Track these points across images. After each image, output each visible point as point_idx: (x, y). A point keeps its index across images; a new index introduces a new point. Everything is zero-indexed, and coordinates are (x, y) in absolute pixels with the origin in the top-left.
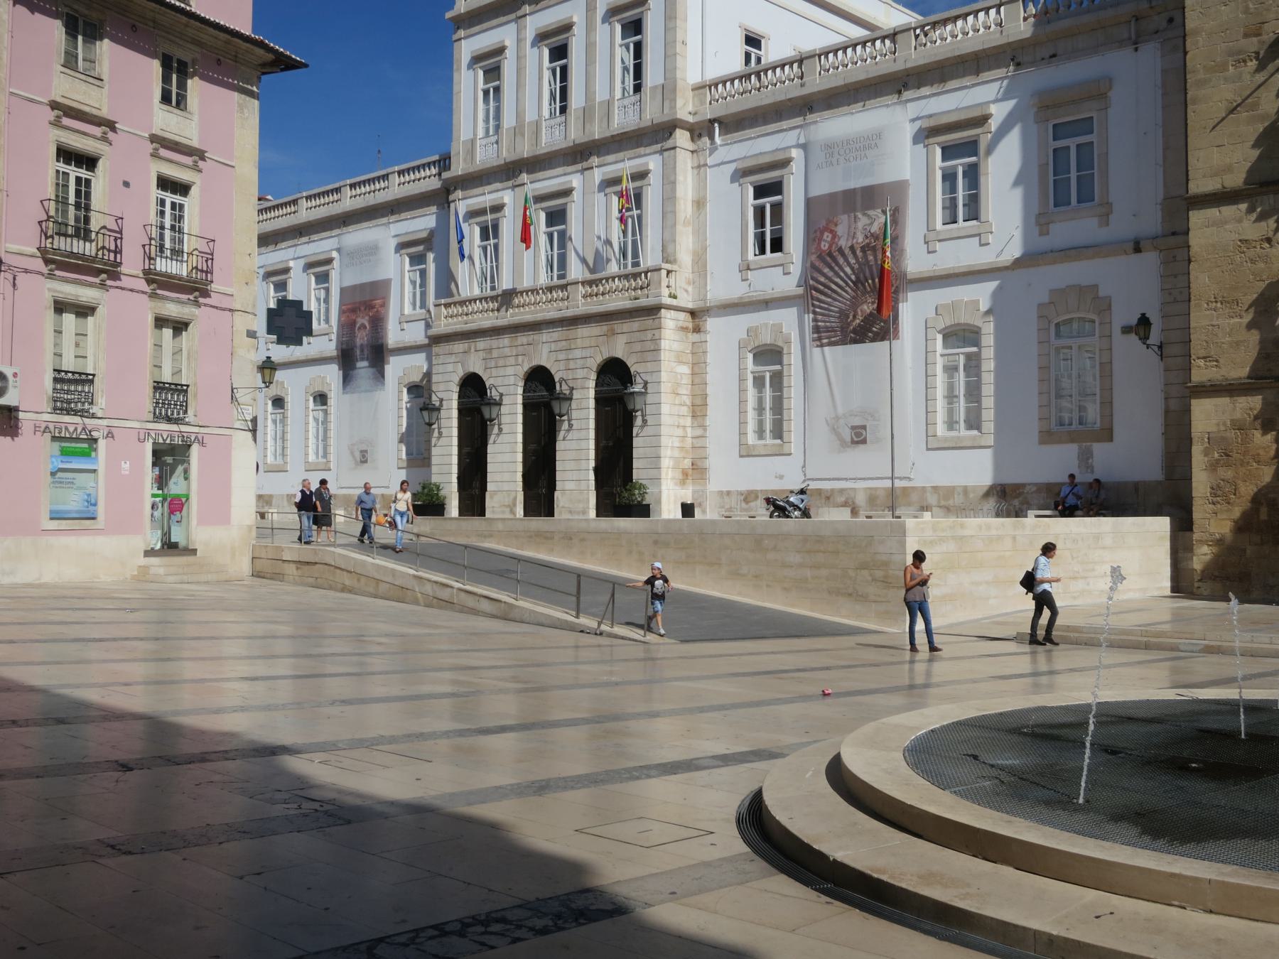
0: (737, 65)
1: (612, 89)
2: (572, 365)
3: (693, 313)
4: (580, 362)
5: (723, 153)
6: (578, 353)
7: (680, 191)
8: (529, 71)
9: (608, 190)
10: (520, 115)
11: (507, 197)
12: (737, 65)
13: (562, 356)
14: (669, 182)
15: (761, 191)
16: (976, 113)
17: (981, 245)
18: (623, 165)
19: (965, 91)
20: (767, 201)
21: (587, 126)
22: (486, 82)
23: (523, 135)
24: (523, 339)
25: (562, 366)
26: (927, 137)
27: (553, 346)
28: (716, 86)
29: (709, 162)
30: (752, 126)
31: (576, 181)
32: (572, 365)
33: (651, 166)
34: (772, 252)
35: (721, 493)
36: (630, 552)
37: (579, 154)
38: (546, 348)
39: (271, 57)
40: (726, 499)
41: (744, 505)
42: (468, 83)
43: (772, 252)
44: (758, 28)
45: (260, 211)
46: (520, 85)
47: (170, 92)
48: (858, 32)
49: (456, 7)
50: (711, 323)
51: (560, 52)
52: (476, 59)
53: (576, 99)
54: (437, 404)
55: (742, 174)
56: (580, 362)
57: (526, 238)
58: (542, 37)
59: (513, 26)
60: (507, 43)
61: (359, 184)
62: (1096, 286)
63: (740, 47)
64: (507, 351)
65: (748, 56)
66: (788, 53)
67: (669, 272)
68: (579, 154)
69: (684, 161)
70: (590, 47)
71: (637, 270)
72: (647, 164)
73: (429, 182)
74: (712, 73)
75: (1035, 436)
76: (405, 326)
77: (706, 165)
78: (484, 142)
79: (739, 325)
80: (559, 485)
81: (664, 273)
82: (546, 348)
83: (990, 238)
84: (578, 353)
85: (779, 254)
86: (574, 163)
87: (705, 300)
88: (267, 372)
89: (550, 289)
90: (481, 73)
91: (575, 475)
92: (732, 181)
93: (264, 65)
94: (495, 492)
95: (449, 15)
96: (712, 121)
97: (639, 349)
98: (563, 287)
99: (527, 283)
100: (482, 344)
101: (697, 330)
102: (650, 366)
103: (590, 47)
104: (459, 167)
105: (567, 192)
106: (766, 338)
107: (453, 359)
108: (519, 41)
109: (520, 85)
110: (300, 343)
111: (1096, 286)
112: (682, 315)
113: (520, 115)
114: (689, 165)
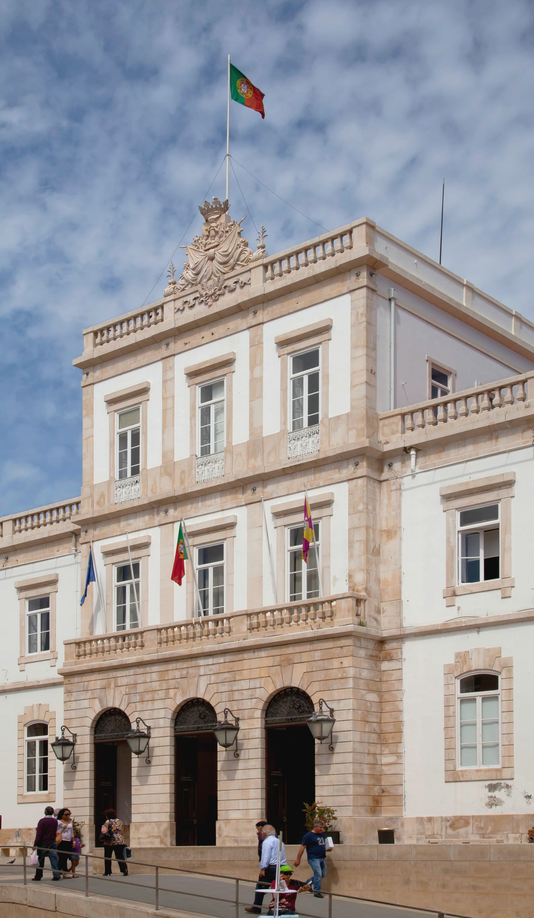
2: (237, 696)
4: (247, 694)
6: (245, 685)
11: (155, 535)
13: (224, 688)
16: (52, 578)
18: (290, 495)
25: (224, 697)
31: (241, 515)
32: (237, 696)
34: (487, 578)
35: (420, 820)
36: (407, 882)
40: (428, 826)
41: (450, 831)
43: (487, 578)
44: (445, 362)
49: (84, 354)
51: (307, 360)
54: (71, 740)
55: (447, 498)
56: (247, 694)
57: (178, 573)
59: (245, 336)
62: (48, 705)
64: (156, 685)
71: (135, 630)
75: (442, 776)
79: (446, 649)
80: (221, 815)
84: (245, 685)
87: (401, 626)
91: (242, 805)
94: (142, 824)
96: (411, 448)
97: (323, 677)
104: (86, 512)
107: (89, 695)
111: (48, 705)
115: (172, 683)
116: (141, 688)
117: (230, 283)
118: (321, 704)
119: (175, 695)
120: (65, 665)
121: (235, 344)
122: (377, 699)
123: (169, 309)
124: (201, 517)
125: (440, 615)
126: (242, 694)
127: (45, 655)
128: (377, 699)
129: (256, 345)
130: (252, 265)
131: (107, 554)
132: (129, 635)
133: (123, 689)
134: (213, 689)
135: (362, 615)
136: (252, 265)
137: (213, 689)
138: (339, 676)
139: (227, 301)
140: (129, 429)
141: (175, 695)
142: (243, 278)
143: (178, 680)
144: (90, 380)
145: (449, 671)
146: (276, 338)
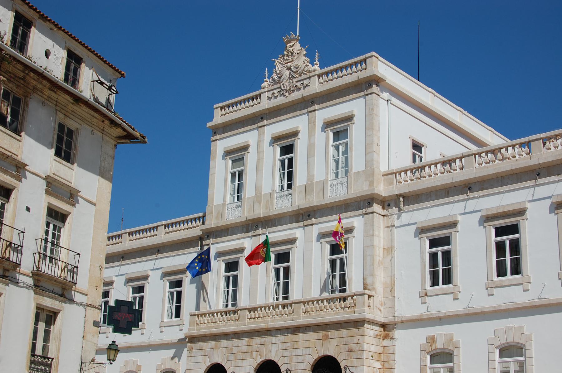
0: (408, 162)
1: (327, 173)
2: (294, 360)
3: (383, 326)
5: (406, 217)
7: (376, 241)
8: (263, 161)
9: (322, 240)
10: (310, 176)
12: (408, 162)
13: (287, 353)
14: (369, 234)
15: (434, 243)
17: (454, 299)
18: (330, 224)
19: (429, 209)
20: (439, 250)
21: (308, 197)
22: (233, 167)
23: (260, 203)
24: (257, 341)
25: (287, 360)
26: (485, 222)
27: (280, 346)
28: (400, 173)
29: (397, 223)
30: (427, 200)
32: (294, 360)
33: (355, 225)
34: (512, 274)
37: (304, 215)
38: (274, 348)
39: (125, 133)
42: (220, 169)
43: (512, 274)
44: (420, 140)
45: (109, 238)
46: (259, 170)
47: (61, 149)
48: (474, 148)
50: (398, 334)
51: (288, 150)
52: (228, 153)
53: (299, 179)
58: (276, 139)
59: (305, 117)
60: (251, 143)
61: (136, 232)
63: (410, 151)
65: (414, 155)
66: (437, 157)
67: (369, 297)
68: (304, 215)
69: (379, 223)
70: (311, 148)
71: (234, 308)
72: (243, 243)
73: (194, 231)
74: (395, 167)
76: (164, 329)
77: (394, 226)
78: (334, 182)
79: (420, 335)
81: (366, 297)
82: (274, 348)
83: (530, 286)
84: (299, 352)
85: (519, 276)
86: (248, 231)
88: (113, 352)
89: (276, 307)
90: (230, 162)
92: (550, 213)
93: (119, 137)
95: (209, 125)
96: (399, 196)
98: (235, 312)
99: (260, 302)
100: (224, 343)
101: (386, 337)
102: (355, 362)
103: (311, 148)
104: (211, 223)
105: (292, 241)
106: (440, 344)
108: (259, 142)
109: (259, 170)
110: (130, 333)
112: (377, 328)
113: (310, 176)
114: (382, 226)
115: (255, 348)
116: (235, 350)
117: (299, 84)
118: (346, 369)
119: (256, 357)
120: (189, 330)
121: (297, 122)
122: (380, 367)
123: (264, 97)
124: (276, 234)
125: (415, 309)
126: (298, 359)
127: (177, 321)
128: (380, 367)
129: (312, 123)
130: (311, 74)
131: (219, 254)
132: (230, 311)
133: (224, 350)
134: (280, 353)
135: (372, 306)
136: (311, 74)
137: (280, 353)
138: (357, 349)
139: (296, 95)
140: (237, 170)
141: (256, 357)
142: (306, 82)
143: (375, 370)
144: (214, 138)
145: (422, 349)
146: (324, 120)
